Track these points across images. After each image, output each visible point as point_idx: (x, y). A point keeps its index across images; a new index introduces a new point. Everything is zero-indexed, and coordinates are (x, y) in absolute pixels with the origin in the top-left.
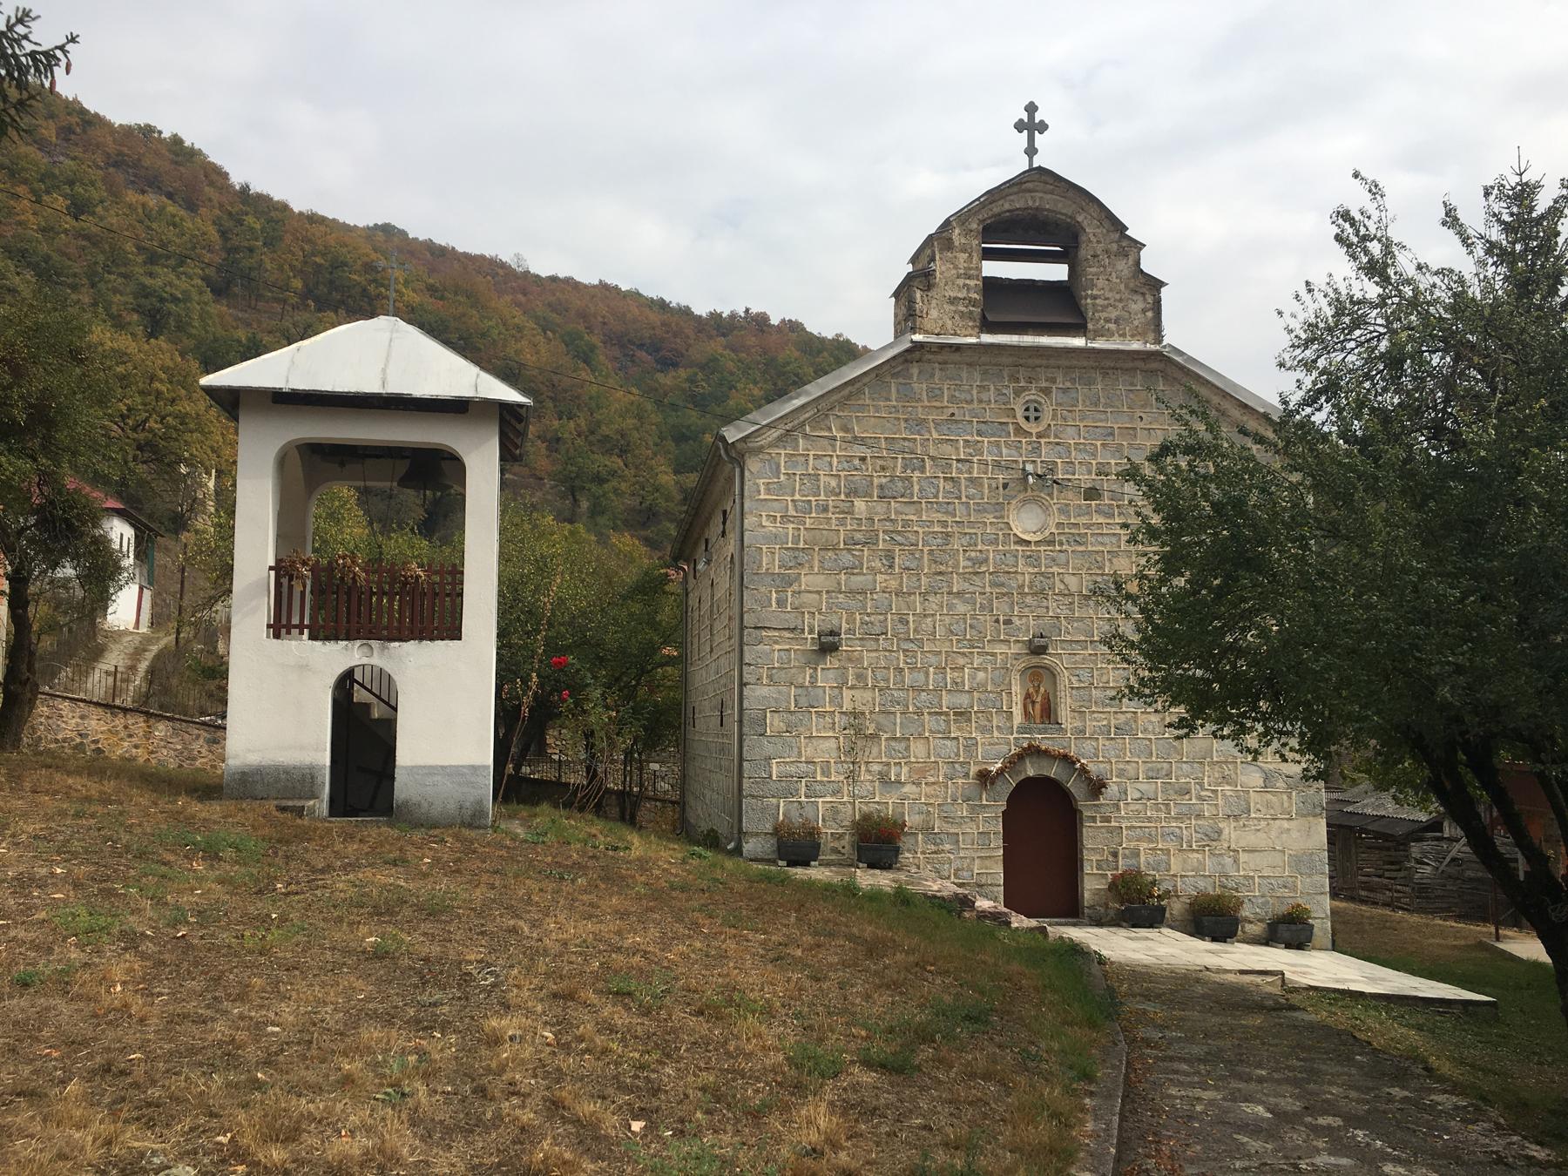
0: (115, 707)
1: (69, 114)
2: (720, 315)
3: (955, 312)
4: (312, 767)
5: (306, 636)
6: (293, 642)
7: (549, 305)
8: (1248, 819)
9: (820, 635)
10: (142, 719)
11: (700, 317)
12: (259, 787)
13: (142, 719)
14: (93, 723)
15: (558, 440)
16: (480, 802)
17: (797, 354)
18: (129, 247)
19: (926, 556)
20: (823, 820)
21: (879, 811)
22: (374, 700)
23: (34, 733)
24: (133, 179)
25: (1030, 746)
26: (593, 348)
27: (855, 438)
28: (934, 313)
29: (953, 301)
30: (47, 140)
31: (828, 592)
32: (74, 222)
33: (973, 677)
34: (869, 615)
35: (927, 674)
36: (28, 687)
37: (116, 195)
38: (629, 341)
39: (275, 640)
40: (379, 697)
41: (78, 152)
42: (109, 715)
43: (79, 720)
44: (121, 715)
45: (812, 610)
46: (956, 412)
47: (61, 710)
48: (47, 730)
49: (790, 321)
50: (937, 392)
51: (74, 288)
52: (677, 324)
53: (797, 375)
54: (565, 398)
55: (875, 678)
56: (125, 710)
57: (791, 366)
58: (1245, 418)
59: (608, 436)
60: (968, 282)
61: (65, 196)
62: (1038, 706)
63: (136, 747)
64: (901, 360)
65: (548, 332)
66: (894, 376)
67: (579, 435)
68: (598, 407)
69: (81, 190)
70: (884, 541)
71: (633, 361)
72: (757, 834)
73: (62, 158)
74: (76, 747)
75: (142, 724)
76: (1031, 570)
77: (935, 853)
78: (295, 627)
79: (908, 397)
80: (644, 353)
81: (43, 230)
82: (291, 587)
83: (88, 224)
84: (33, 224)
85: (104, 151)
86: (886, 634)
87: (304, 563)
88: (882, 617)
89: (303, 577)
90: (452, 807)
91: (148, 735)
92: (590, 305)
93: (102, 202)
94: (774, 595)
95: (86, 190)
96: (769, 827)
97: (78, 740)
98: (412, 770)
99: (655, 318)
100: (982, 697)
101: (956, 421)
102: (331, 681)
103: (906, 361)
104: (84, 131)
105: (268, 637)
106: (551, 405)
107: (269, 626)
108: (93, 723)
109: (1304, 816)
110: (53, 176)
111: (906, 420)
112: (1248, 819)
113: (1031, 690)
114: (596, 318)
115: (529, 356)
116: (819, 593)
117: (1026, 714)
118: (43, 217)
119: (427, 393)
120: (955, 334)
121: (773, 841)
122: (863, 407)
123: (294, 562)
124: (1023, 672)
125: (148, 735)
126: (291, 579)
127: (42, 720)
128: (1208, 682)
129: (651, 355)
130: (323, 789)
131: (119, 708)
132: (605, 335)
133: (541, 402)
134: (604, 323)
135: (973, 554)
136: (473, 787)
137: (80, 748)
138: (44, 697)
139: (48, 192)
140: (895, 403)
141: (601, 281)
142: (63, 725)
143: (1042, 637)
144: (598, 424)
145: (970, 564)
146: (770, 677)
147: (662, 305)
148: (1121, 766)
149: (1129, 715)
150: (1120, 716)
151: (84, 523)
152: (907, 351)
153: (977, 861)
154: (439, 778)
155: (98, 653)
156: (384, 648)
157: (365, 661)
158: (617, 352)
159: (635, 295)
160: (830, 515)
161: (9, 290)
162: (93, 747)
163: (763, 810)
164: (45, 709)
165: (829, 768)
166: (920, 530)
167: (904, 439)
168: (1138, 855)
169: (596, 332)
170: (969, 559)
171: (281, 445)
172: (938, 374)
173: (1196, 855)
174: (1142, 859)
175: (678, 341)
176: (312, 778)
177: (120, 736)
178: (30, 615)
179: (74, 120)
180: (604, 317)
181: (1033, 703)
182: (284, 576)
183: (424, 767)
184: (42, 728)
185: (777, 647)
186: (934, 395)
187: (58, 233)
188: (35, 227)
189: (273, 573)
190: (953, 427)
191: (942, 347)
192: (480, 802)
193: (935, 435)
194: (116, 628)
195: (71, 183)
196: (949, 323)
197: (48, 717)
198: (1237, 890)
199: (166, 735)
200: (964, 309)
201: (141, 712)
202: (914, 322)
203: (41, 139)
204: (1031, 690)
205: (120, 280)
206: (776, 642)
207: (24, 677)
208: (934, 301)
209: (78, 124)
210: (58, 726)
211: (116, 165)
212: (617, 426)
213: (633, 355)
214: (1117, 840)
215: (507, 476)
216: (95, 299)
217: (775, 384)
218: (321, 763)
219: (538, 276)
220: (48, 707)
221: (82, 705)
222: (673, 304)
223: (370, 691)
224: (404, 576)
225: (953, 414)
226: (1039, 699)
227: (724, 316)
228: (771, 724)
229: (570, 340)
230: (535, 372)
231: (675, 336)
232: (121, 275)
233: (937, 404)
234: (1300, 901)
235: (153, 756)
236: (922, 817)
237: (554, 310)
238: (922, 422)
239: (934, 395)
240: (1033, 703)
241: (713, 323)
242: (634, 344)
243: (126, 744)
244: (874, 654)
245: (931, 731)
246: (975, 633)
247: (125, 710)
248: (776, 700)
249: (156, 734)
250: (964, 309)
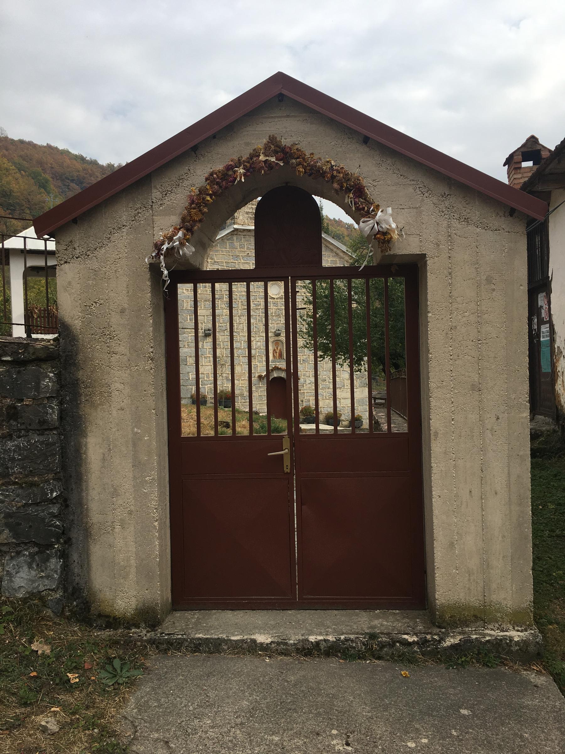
2: (113, 166)
3: (248, 217)
7: (21, 156)
8: (344, 388)
9: (205, 331)
11: (103, 166)
19: (240, 303)
20: (207, 393)
21: (226, 389)
25: (275, 367)
26: (47, 181)
27: (215, 262)
28: (241, 217)
29: (247, 213)
31: (207, 316)
33: (256, 344)
34: (221, 323)
35: (241, 343)
38: (66, 178)
45: (202, 322)
46: (249, 253)
50: (243, 246)
52: (91, 170)
54: (36, 208)
55: (224, 345)
58: (344, 256)
60: (252, 206)
62: (278, 354)
64: (230, 234)
65: (22, 171)
66: (228, 240)
70: (226, 298)
71: (69, 189)
72: (185, 398)
76: (275, 308)
77: (244, 402)
79: (233, 247)
80: (74, 185)
86: (227, 330)
88: (225, 324)
92: (43, 157)
94: (189, 317)
96: (189, 396)
99: (79, 166)
100: (259, 351)
101: (249, 256)
103: (232, 235)
109: (361, 387)
111: (232, 256)
112: (344, 388)
113: (275, 348)
114: (47, 164)
115: (14, 185)
116: (204, 316)
117: (274, 356)
120: (249, 225)
121: (191, 400)
122: (217, 251)
124: (273, 342)
128: (328, 344)
129: (78, 185)
132: (53, 174)
134: (52, 168)
135: (256, 302)
140: (228, 250)
141: (47, 144)
143: (279, 330)
145: (255, 306)
146: (188, 345)
147: (82, 159)
148: (304, 373)
149: (307, 356)
150: (304, 356)
152: (232, 231)
153: (258, 405)
158: (60, 184)
159: (66, 153)
160: (207, 289)
163: (187, 390)
165: (209, 375)
166: (238, 294)
167: (232, 262)
168: (309, 401)
169: (48, 172)
170: (254, 304)
172: (243, 239)
173: (328, 401)
174: (311, 402)
175: (92, 178)
180: (51, 164)
181: (276, 352)
185: (190, 335)
186: (242, 247)
190: (248, 258)
191: (244, 230)
193: (242, 261)
196: (246, 221)
198: (340, 411)
200: (251, 216)
202: (234, 221)
204: (275, 348)
206: (190, 333)
208: (241, 213)
213: (69, 185)
214: (303, 396)
219: (12, 140)
222: (88, 159)
225: (248, 254)
226: (278, 351)
227: (115, 166)
228: (189, 361)
229: (35, 176)
230: (19, 194)
231: (91, 176)
233: (243, 250)
234: (359, 414)
236: (240, 391)
237: (24, 160)
238: (237, 256)
239: (242, 247)
240: (276, 352)
241: (109, 169)
242: (69, 179)
244: (223, 337)
245: (242, 362)
246: (257, 329)
248: (190, 353)
250: (251, 216)
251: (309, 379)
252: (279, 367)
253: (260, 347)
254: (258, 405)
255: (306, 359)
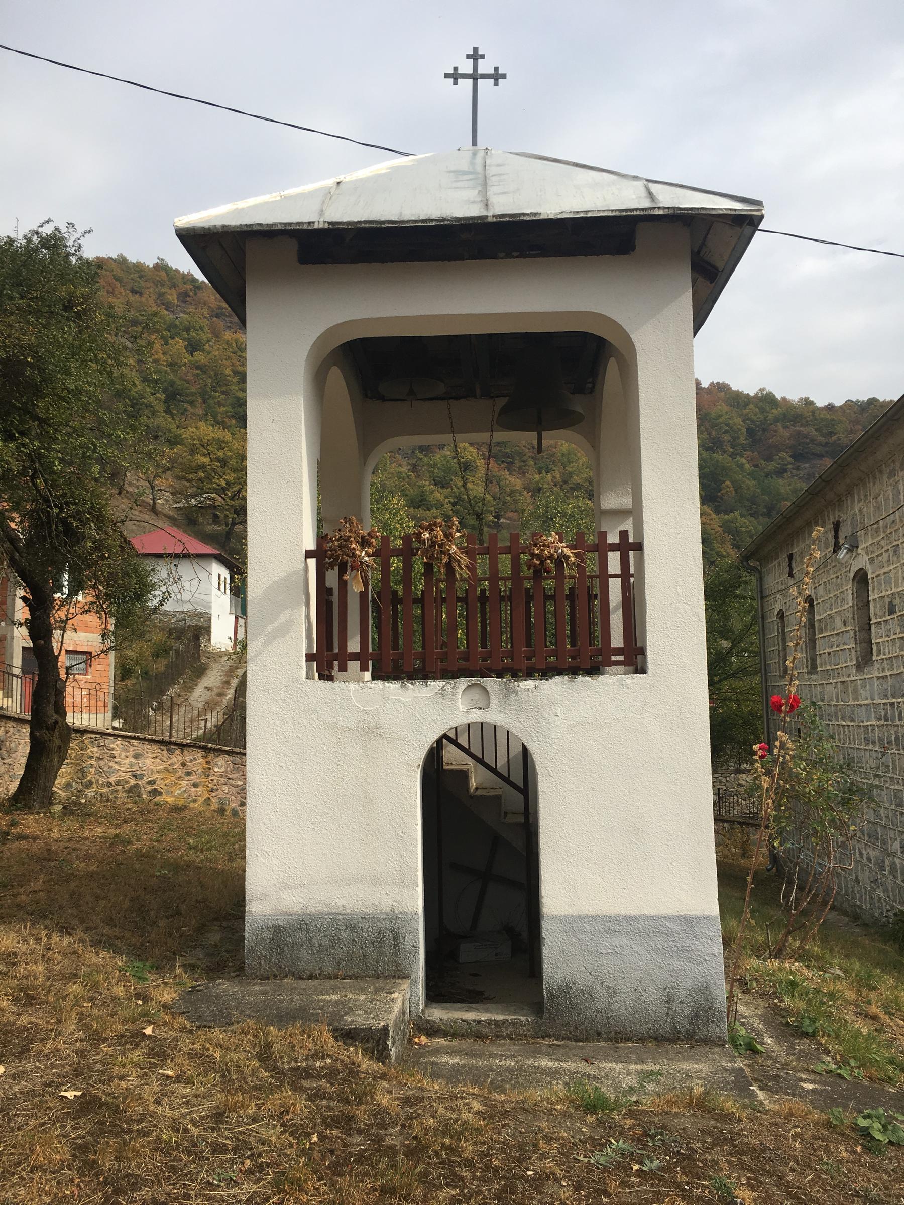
0: (170, 743)
1: (185, 283)
4: (394, 917)
5: (367, 675)
6: (352, 686)
10: (200, 755)
12: (305, 955)
13: (200, 755)
14: (148, 762)
15: (540, 489)
16: (704, 990)
17: (726, 408)
18: (228, 371)
22: (471, 762)
23: (84, 777)
24: (229, 325)
30: (170, 302)
32: (190, 358)
36: (57, 732)
37: (217, 335)
39: (322, 683)
40: (480, 761)
41: (191, 309)
42: (165, 752)
43: (133, 760)
44: (178, 752)
47: (113, 749)
48: (99, 772)
49: (718, 383)
51: (191, 403)
53: (727, 425)
56: (182, 746)
57: (723, 418)
59: (578, 484)
61: (184, 340)
63: (195, 785)
67: (555, 485)
68: (569, 462)
69: (194, 334)
73: (182, 315)
74: (130, 790)
75: (201, 760)
78: (354, 657)
81: (171, 365)
82: (343, 585)
83: (199, 357)
84: (164, 361)
85: (209, 307)
87: (364, 543)
89: (359, 566)
90: (652, 997)
91: (207, 771)
93: (208, 341)
95: (197, 335)
97: (133, 782)
98: (573, 923)
102: (419, 756)
104: (196, 294)
105: (309, 677)
106: (532, 463)
107: (310, 657)
108: (148, 762)
110: (176, 326)
118: (170, 355)
119: (567, 209)
123: (347, 540)
125: (207, 771)
126: (342, 572)
127: (93, 762)
130: (416, 958)
131: (175, 744)
133: (524, 462)
136: (690, 960)
137: (134, 791)
138: (93, 736)
139: (173, 338)
142: (116, 767)
144: (570, 474)
151: (84, 523)
154: (625, 940)
155: (201, 672)
156: (508, 692)
157: (476, 716)
161: (147, 406)
162: (149, 788)
164: (96, 749)
171: (313, 338)
176: (396, 938)
177: (177, 775)
178: (55, 645)
179: (189, 287)
182: (332, 566)
183: (594, 918)
184: (93, 770)
187: (180, 366)
188: (165, 363)
189: (312, 563)
192: (704, 990)
194: (219, 650)
195: (188, 330)
197: (99, 759)
199: (226, 772)
201: (199, 747)
203: (167, 303)
205: (223, 396)
207: (52, 721)
209: (191, 290)
210: (110, 767)
211: (217, 316)
212: (585, 475)
215: (501, 520)
216: (206, 411)
217: (710, 434)
218: (409, 909)
220: (98, 746)
221: (135, 742)
223: (467, 751)
224: (539, 557)
232: (223, 392)
235: (214, 794)
243: (184, 783)
247: (182, 746)
249: (216, 770)
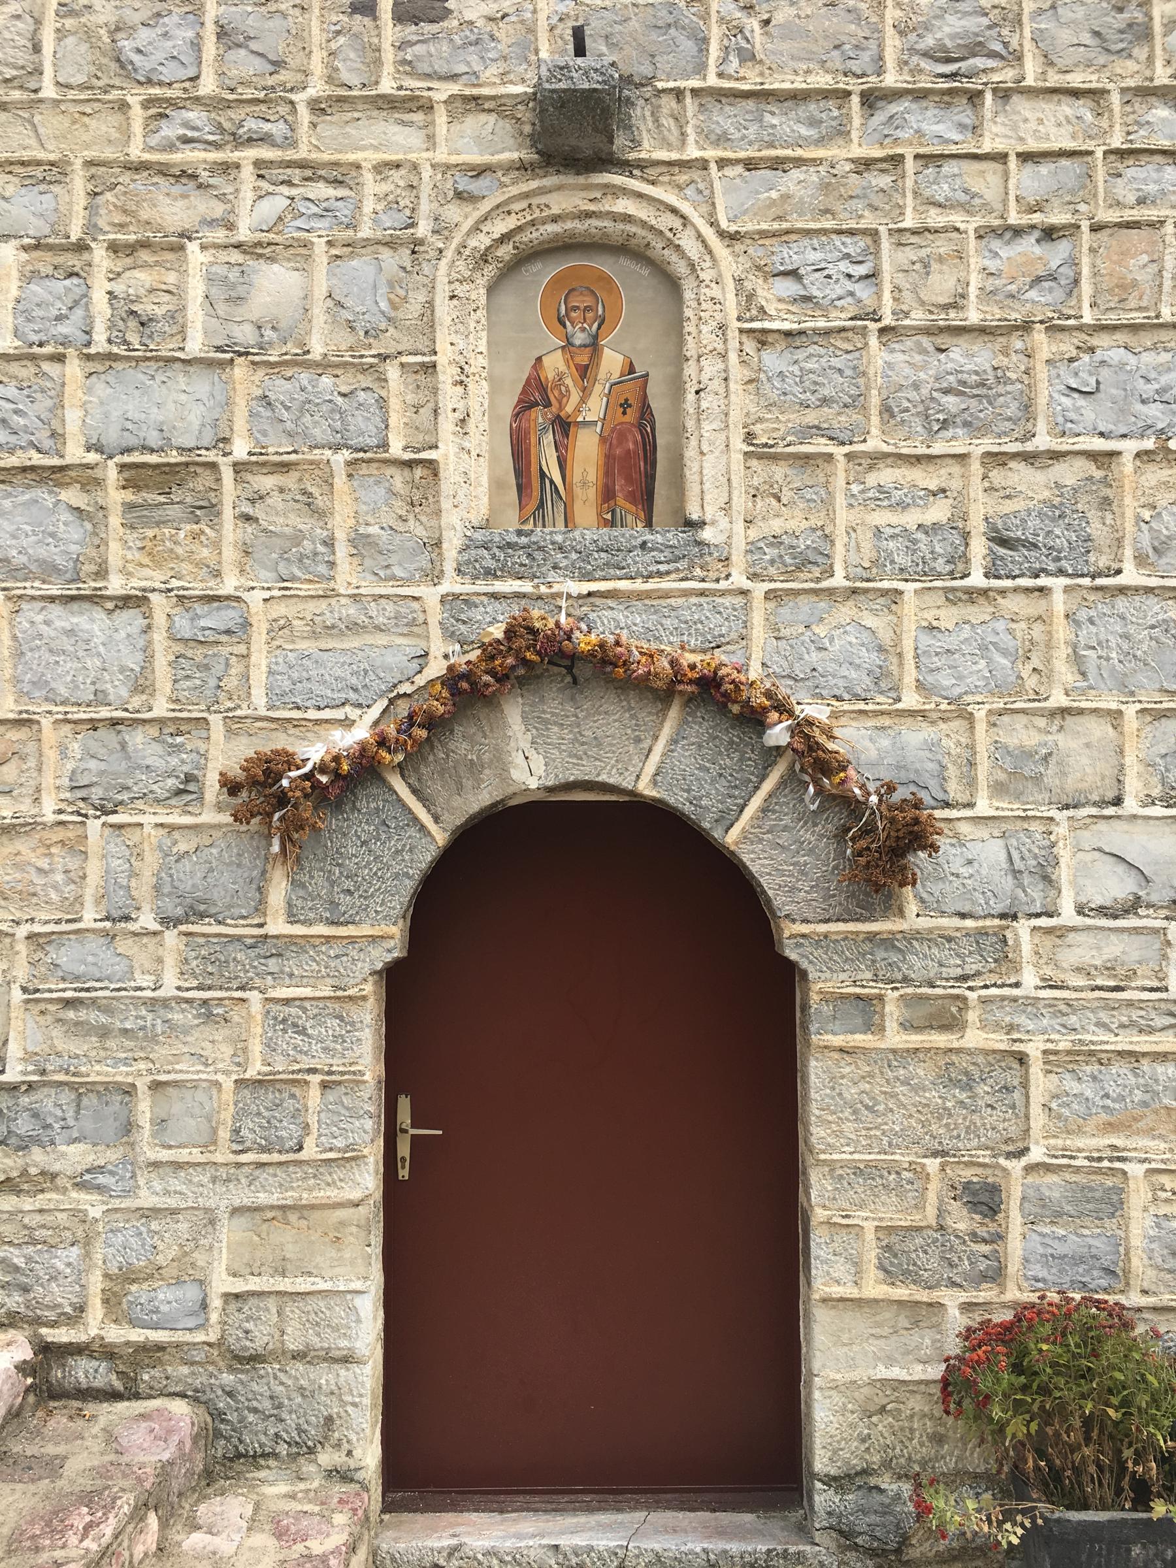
100: (280, 389)
113: (555, 364)
149: (1069, 473)
150: (1020, 476)
153: (228, 1232)
181: (564, 427)
204: (555, 364)
214: (1000, 1122)
226: (595, 409)
240: (564, 427)
251: (1115, 837)
252: (584, 642)
253: (296, 333)
254: (228, 1232)
255: (1057, 512)
